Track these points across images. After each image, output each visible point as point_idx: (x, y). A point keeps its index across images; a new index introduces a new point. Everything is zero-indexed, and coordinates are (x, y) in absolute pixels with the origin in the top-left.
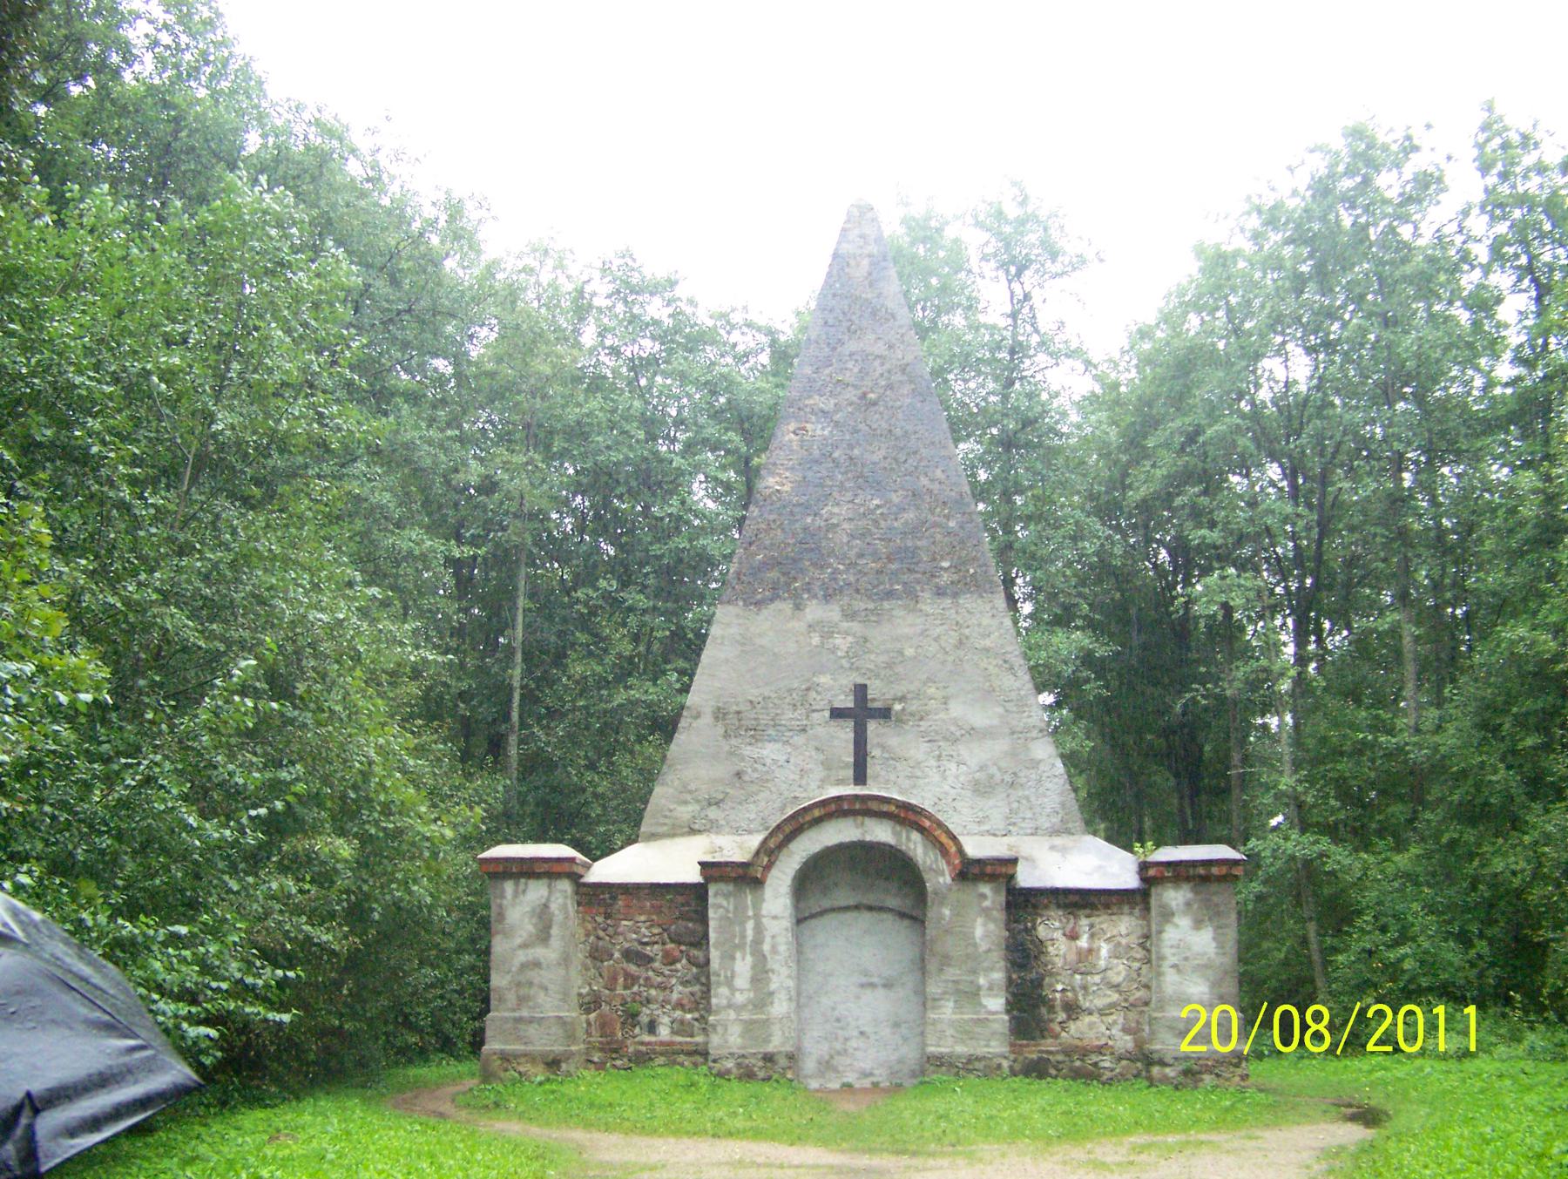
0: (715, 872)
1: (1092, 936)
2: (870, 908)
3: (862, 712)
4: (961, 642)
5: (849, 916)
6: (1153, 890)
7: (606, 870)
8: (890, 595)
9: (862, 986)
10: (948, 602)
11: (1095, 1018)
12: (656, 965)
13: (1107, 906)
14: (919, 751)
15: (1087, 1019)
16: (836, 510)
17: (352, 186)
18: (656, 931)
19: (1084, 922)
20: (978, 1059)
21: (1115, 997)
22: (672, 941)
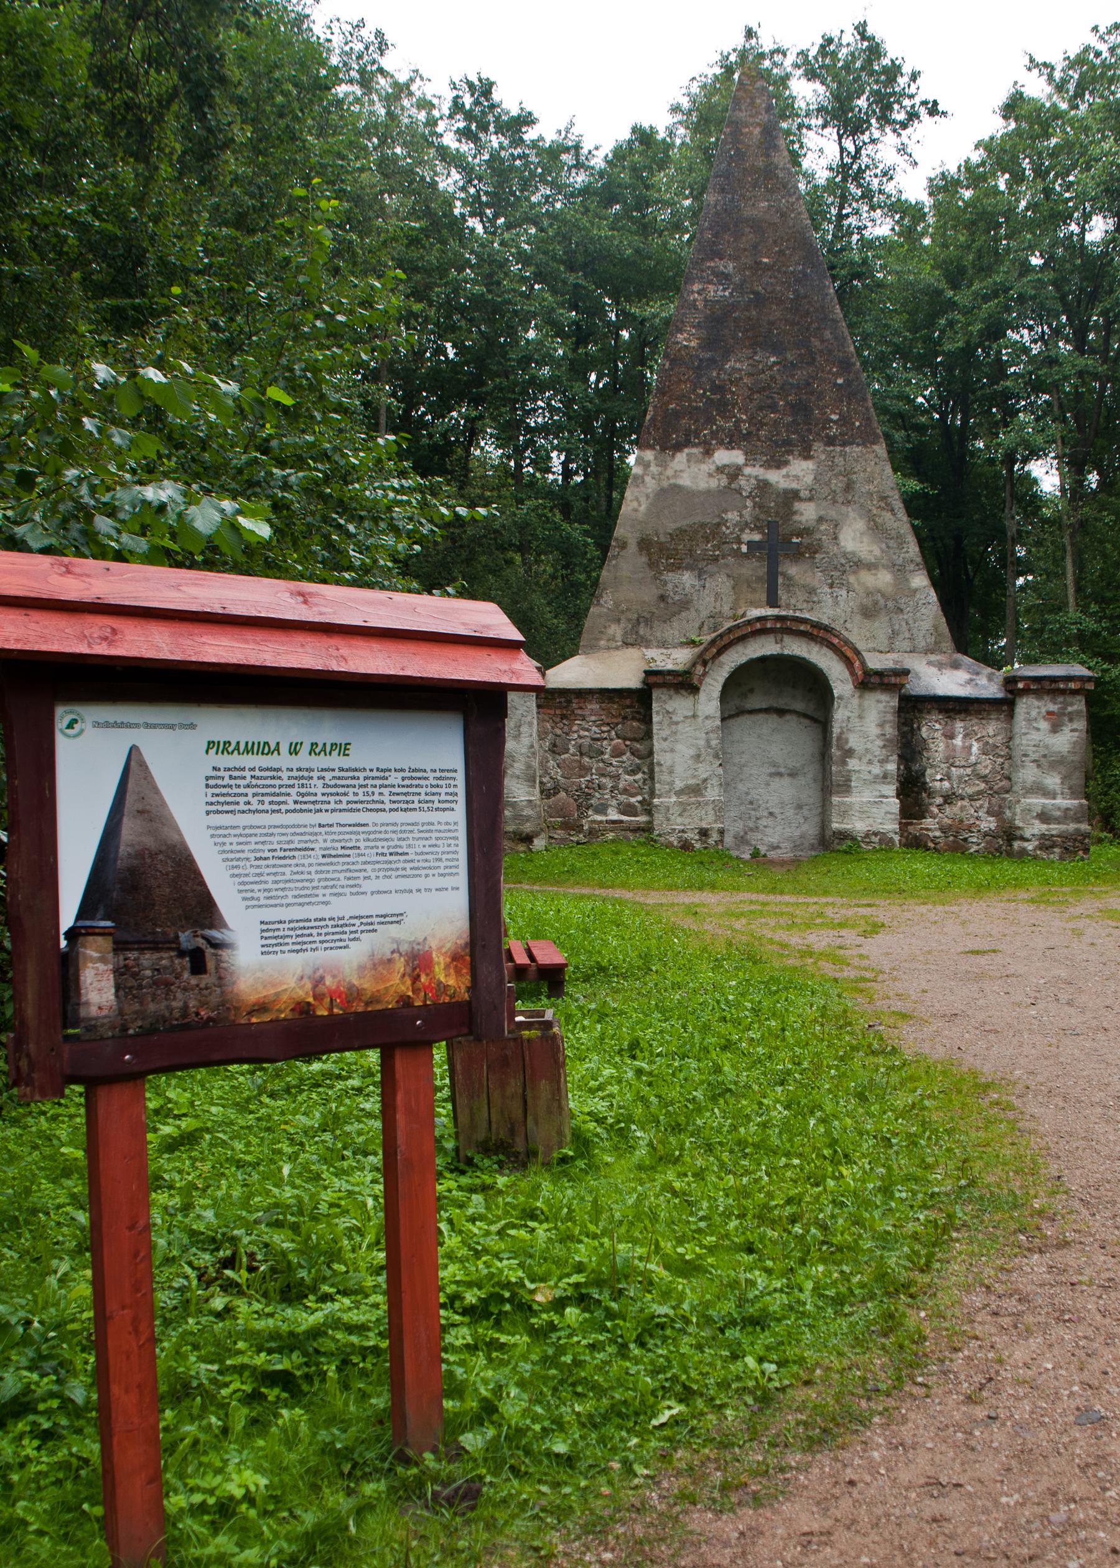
0: (658, 679)
1: (966, 736)
5: (761, 717)
6: (1018, 700)
9: (771, 775)
11: (965, 803)
13: (978, 712)
14: (816, 579)
16: (738, 365)
18: (605, 729)
19: (959, 726)
20: (875, 834)
21: (983, 786)
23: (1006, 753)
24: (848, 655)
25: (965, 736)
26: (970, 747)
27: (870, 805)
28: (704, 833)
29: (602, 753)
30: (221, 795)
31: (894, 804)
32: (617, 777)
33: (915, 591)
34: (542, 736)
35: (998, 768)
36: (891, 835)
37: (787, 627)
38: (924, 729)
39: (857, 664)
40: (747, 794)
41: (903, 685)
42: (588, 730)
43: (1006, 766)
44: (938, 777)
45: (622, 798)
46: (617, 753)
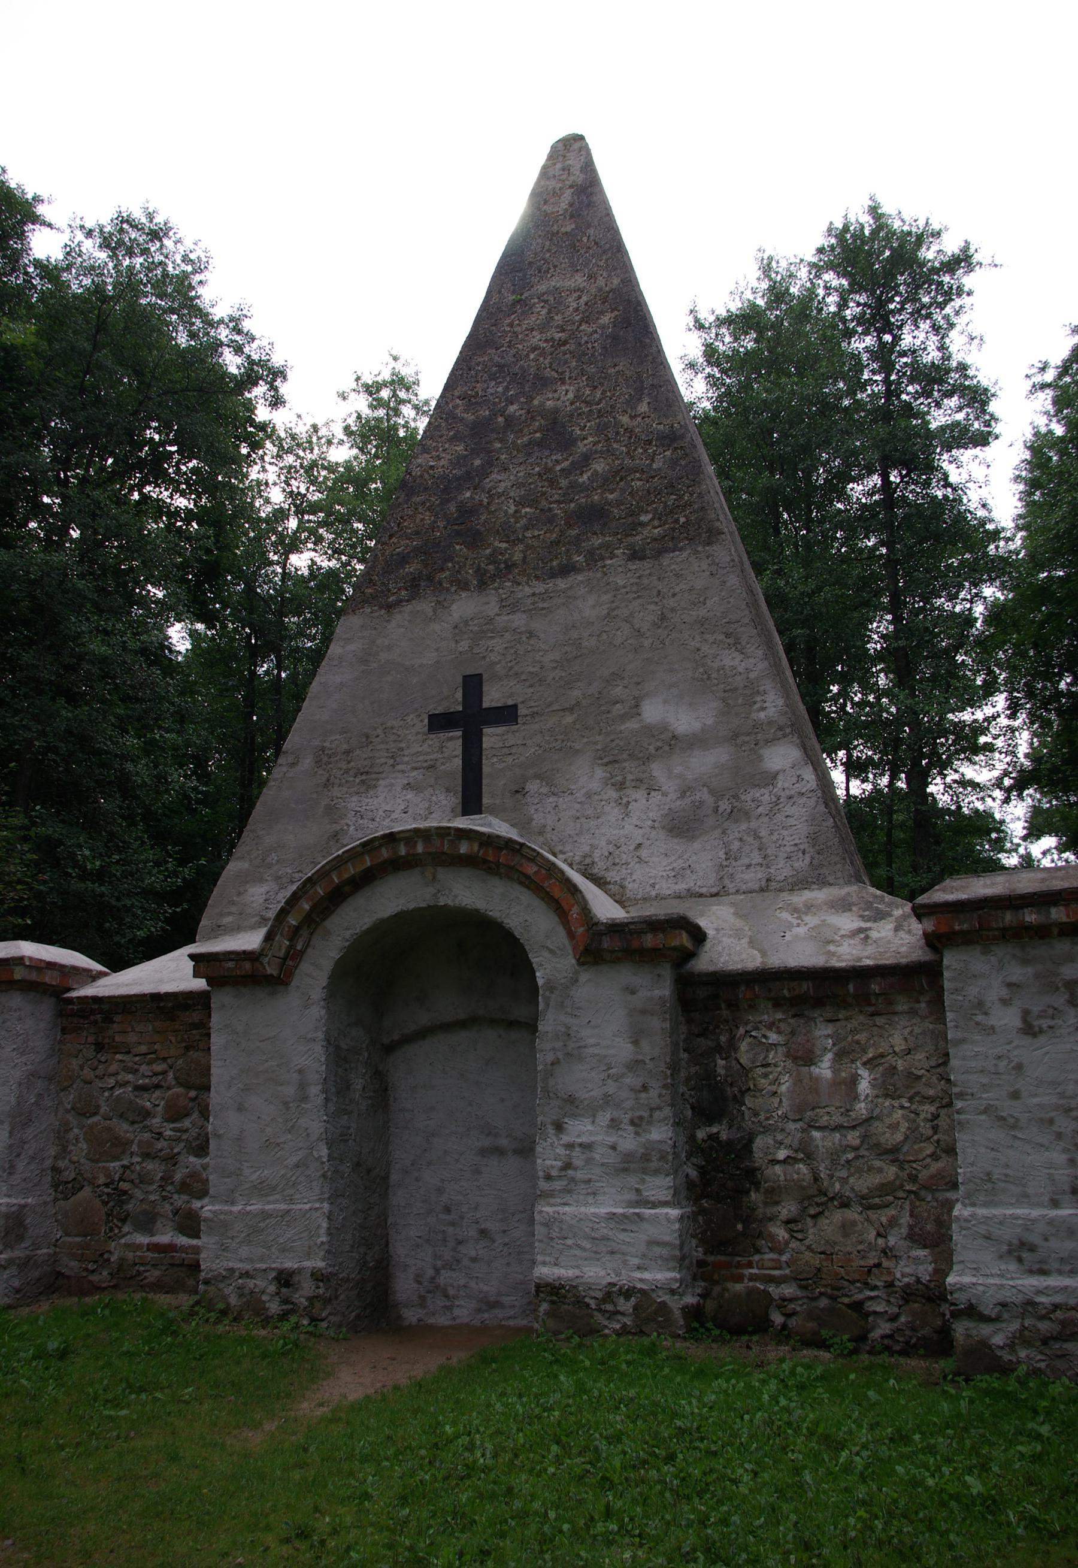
2: (493, 1022)
3: (469, 718)
4: (663, 618)
8: (567, 570)
9: (483, 1152)
10: (647, 564)
11: (852, 1214)
12: (156, 1121)
15: (838, 1216)
17: (46, 270)
19: (823, 1033)
21: (891, 1172)
22: (180, 1084)
23: (936, 1095)
24: (558, 896)
25: (839, 1056)
26: (854, 1080)
28: (285, 1279)
31: (668, 1219)
32: (172, 1159)
33: (775, 776)
37: (498, 859)
38: (744, 1046)
39: (575, 912)
43: (943, 1123)
44: (782, 1154)
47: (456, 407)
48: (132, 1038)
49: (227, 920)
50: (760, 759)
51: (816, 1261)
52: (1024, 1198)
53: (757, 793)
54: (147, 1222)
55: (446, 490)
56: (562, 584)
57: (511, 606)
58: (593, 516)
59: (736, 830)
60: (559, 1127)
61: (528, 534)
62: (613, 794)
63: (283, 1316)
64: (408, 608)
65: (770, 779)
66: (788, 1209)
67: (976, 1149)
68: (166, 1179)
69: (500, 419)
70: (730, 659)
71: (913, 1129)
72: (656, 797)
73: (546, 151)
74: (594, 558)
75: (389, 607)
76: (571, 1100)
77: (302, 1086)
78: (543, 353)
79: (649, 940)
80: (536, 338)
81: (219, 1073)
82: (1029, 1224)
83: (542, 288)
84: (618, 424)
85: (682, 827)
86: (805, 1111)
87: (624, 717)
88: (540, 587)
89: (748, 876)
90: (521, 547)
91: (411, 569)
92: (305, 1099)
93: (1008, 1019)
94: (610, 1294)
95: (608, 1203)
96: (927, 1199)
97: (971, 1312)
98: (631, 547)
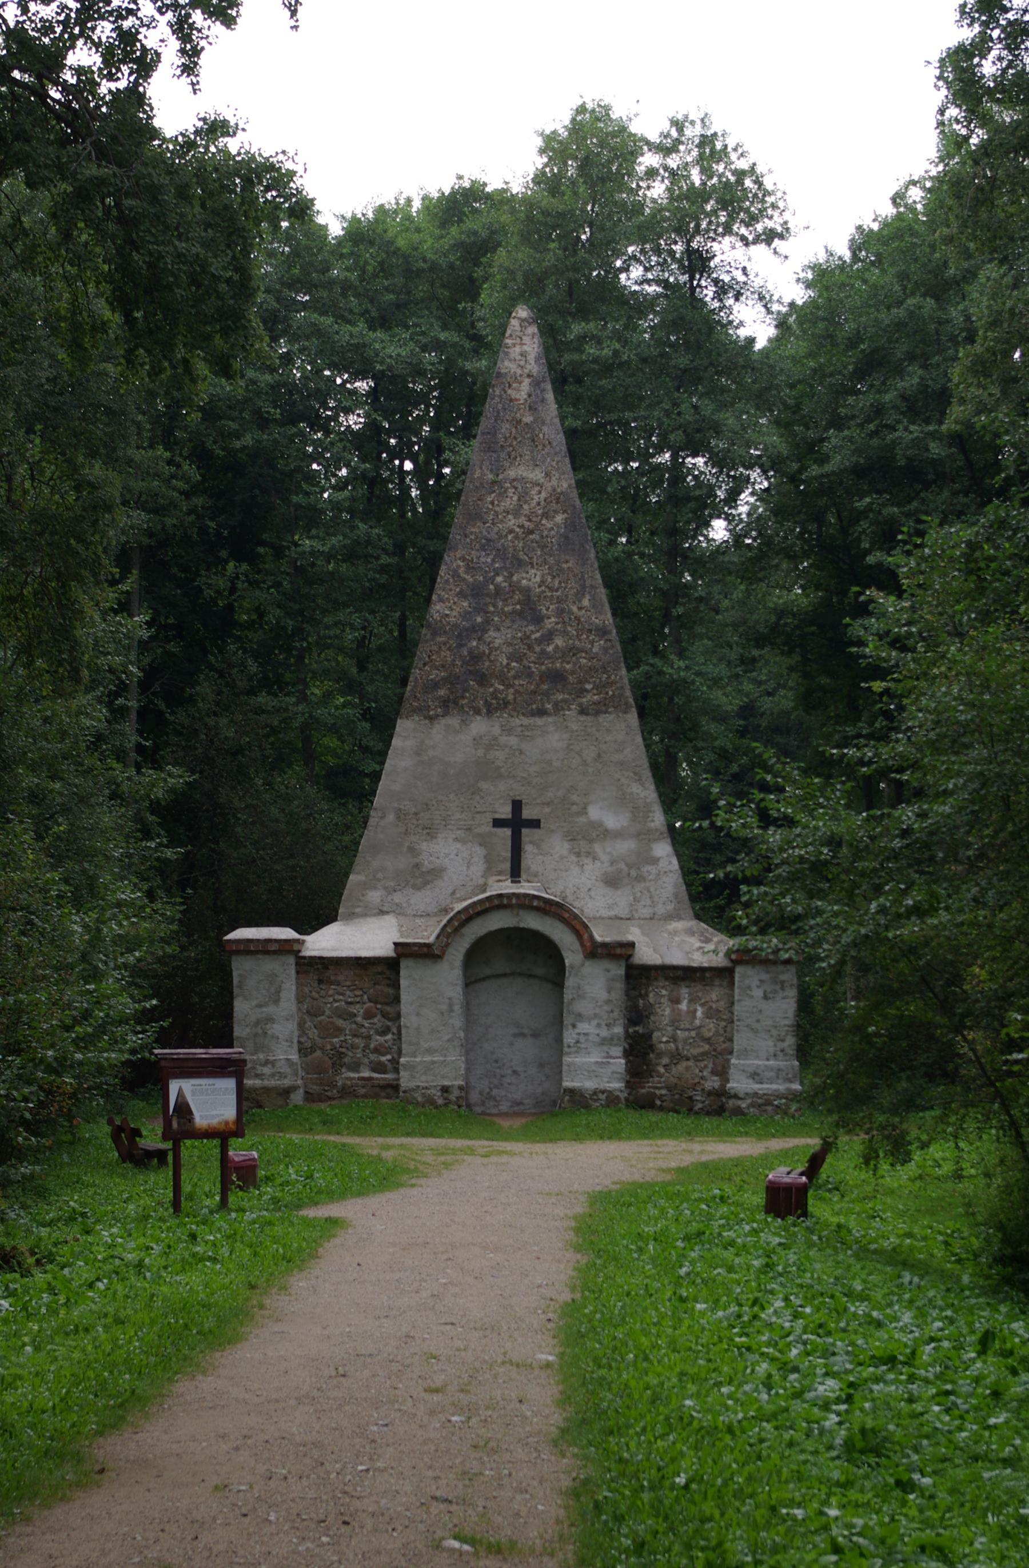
2: (520, 974)
4: (599, 756)
7: (326, 942)
8: (542, 713)
9: (515, 1035)
10: (589, 718)
11: (690, 1063)
12: (359, 1019)
15: (685, 1064)
19: (684, 992)
20: (603, 1092)
21: (707, 1047)
22: (370, 1000)
24: (577, 926)
26: (695, 1011)
27: (594, 1063)
28: (445, 1090)
29: (355, 1015)
30: (194, 1093)
31: (620, 1064)
34: (300, 999)
35: (721, 1031)
36: (618, 1093)
38: (651, 995)
39: (586, 936)
40: (492, 1053)
41: (630, 956)
42: (343, 994)
43: (729, 1029)
44: (664, 1039)
45: (373, 1057)
46: (369, 1015)
47: (459, 567)
48: (341, 978)
49: (358, 910)
50: (651, 849)
51: (675, 1081)
52: (757, 1057)
53: (649, 868)
54: (355, 1067)
55: (459, 636)
56: (539, 721)
57: (508, 731)
58: (557, 678)
59: (639, 887)
60: (574, 1026)
61: (517, 682)
62: (574, 858)
63: (446, 1105)
64: (443, 721)
65: (655, 861)
66: (665, 1060)
67: (740, 1041)
68: (367, 1046)
69: (491, 587)
70: (636, 789)
71: (717, 1031)
72: (598, 864)
73: (441, 183)
74: (558, 708)
75: (431, 719)
76: (580, 1015)
77: (451, 1005)
78: (517, 537)
79: (618, 951)
80: (512, 522)
81: (404, 996)
82: (758, 1066)
83: (512, 473)
84: (570, 612)
85: (612, 881)
86: (675, 1022)
87: (579, 814)
88: (525, 721)
89: (644, 911)
90: (512, 690)
91: (442, 692)
92: (452, 1011)
93: (758, 993)
94: (595, 1092)
95: (594, 1057)
96: (720, 1059)
97: (736, 1096)
98: (580, 705)
